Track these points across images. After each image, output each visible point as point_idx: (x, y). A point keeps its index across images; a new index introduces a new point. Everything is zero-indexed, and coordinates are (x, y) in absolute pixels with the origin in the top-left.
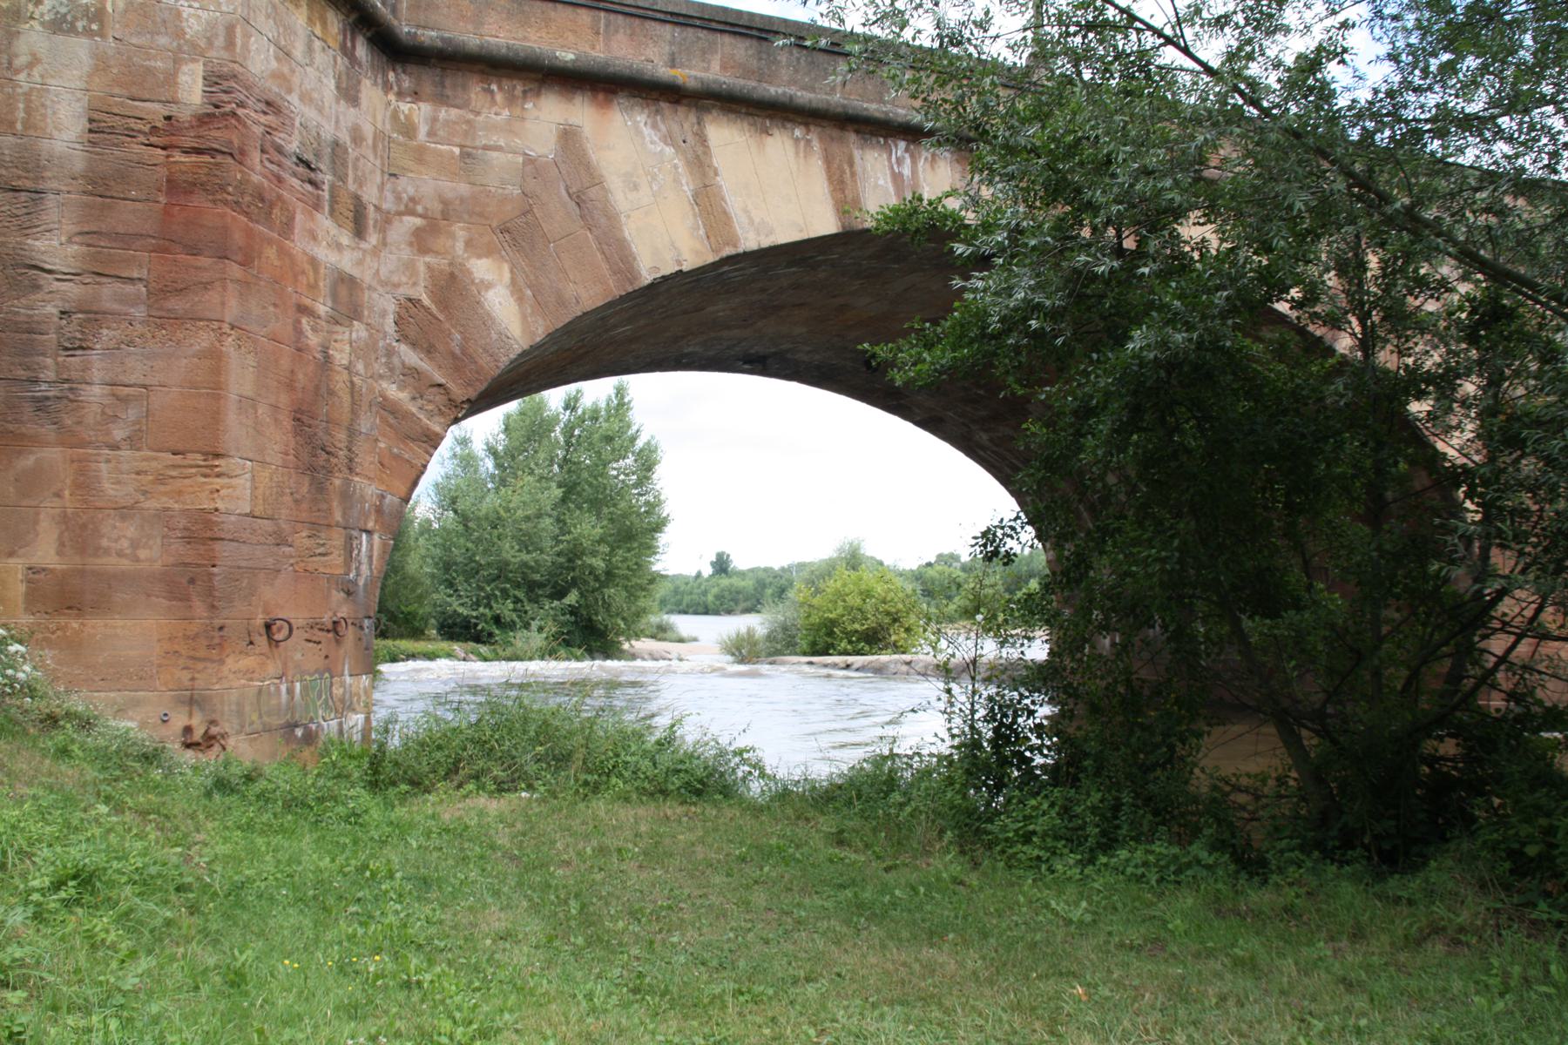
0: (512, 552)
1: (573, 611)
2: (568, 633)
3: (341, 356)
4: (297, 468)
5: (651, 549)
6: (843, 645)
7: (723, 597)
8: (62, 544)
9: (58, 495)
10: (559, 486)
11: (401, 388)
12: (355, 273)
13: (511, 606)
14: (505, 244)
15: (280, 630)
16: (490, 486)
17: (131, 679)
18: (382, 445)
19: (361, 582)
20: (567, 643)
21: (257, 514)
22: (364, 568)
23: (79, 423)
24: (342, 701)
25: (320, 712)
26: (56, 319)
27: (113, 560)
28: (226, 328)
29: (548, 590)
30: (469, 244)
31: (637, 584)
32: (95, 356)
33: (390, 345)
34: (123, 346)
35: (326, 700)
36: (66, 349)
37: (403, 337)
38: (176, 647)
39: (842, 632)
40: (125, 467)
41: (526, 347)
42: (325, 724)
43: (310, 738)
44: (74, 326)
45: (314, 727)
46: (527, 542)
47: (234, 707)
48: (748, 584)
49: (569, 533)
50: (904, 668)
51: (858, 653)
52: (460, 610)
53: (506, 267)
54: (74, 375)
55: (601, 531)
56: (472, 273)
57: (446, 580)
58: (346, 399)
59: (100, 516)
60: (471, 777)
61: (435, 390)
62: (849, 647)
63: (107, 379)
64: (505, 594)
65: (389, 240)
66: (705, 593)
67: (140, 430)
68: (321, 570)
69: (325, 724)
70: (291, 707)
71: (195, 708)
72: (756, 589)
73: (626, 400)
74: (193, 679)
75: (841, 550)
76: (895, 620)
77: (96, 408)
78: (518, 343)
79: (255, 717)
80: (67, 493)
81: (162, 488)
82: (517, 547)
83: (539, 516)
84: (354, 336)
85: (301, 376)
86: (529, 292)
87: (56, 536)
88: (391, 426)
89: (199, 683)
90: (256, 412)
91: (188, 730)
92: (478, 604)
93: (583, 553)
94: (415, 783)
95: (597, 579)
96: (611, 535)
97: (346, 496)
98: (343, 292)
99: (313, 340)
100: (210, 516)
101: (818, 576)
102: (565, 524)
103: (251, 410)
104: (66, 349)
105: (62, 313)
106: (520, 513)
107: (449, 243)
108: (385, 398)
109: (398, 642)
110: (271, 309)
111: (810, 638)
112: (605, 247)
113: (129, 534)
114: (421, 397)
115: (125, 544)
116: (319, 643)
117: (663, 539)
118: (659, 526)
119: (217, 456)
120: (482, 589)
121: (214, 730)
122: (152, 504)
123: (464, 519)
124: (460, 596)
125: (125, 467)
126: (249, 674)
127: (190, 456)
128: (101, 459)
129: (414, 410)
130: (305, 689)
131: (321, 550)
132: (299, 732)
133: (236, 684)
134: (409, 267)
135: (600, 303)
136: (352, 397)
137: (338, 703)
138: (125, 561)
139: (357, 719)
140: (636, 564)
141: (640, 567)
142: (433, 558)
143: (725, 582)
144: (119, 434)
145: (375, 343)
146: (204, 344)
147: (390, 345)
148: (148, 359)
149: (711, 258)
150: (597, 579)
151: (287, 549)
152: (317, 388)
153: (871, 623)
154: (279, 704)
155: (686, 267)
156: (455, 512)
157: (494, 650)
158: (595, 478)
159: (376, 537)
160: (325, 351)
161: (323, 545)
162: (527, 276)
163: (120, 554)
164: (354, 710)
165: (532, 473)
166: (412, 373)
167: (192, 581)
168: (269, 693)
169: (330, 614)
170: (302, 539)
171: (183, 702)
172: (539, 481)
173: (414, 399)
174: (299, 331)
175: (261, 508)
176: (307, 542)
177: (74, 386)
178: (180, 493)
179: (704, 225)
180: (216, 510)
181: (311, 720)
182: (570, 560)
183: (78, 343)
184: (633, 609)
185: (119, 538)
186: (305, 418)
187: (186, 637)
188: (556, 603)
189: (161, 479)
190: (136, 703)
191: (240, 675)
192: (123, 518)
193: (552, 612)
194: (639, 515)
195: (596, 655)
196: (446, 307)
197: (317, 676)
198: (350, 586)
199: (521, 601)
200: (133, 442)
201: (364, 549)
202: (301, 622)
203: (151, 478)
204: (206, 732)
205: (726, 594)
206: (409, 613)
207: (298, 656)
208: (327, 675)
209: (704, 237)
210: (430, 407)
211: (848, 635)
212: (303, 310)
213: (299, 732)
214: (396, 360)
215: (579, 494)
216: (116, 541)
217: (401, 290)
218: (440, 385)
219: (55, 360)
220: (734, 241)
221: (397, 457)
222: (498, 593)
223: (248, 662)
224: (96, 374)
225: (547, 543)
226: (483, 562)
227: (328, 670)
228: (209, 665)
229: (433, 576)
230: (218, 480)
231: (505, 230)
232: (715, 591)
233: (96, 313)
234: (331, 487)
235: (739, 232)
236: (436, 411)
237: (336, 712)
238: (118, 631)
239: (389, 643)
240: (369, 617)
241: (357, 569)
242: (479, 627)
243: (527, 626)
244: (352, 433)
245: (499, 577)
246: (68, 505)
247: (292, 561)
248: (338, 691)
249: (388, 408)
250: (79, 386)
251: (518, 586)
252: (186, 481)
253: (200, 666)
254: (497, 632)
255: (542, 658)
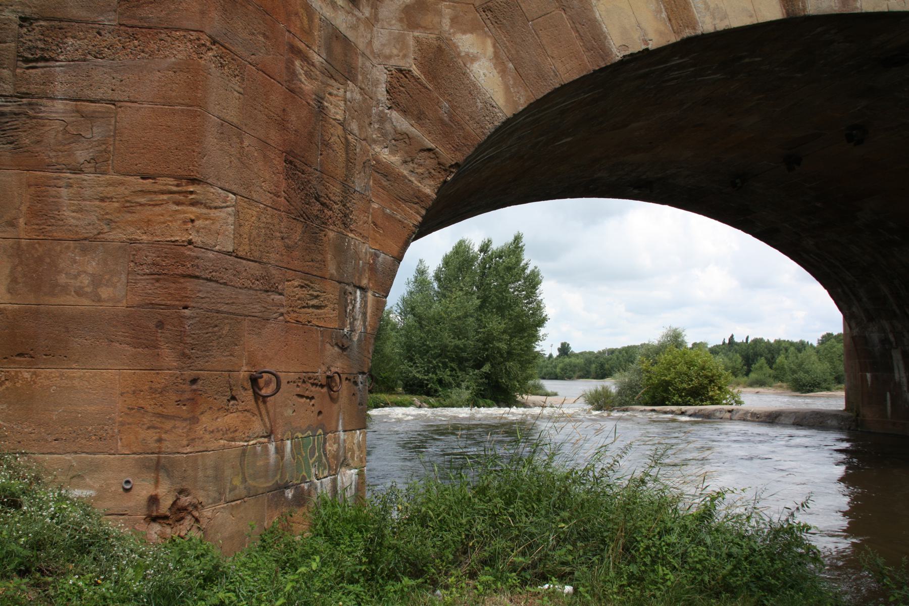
0: (449, 339)
1: (487, 376)
2: (483, 391)
3: (336, 110)
4: (288, 212)
5: (534, 337)
6: (675, 398)
7: (566, 369)
8: (14, 280)
9: (12, 224)
10: (478, 298)
11: (393, 153)
12: (349, 34)
13: (449, 373)
14: (488, 22)
15: (268, 384)
16: (435, 299)
17: (89, 439)
18: (376, 206)
19: (355, 339)
20: (484, 397)
21: (240, 254)
22: (359, 324)
23: (38, 142)
24: (336, 457)
25: (313, 470)
26: (16, 26)
27: (72, 299)
28: (205, 39)
29: (471, 363)
30: (454, 20)
31: (526, 359)
32: (58, 70)
33: (382, 111)
34: (89, 57)
35: (320, 457)
36: (27, 60)
37: (395, 105)
38: (141, 402)
39: (674, 389)
40: (88, 193)
41: (509, 115)
42: (318, 482)
43: (301, 499)
44: (35, 34)
45: (306, 486)
46: (459, 333)
47: (210, 472)
48: (581, 361)
49: (485, 327)
50: (728, 415)
51: (686, 404)
52: (417, 375)
53: (489, 42)
54: (34, 89)
55: (504, 326)
56: (457, 47)
57: (409, 357)
58: (341, 156)
59: (58, 248)
60: (484, 563)
61: (425, 154)
62: (680, 400)
63: (72, 94)
64: (445, 366)
65: (381, 16)
66: (555, 367)
67: (105, 151)
68: (315, 322)
69: (318, 482)
70: (280, 467)
71: (162, 474)
72: (585, 364)
73: (520, 245)
74: (160, 440)
75: (667, 336)
76: (711, 381)
77: (58, 126)
78: (502, 111)
79: (237, 482)
80: (22, 221)
81: (129, 217)
82: (452, 336)
83: (466, 316)
84: (348, 95)
85: (293, 118)
86: (511, 65)
87: (7, 271)
88: (384, 188)
89: (167, 446)
90: (242, 142)
91: (154, 500)
92: (428, 372)
93: (493, 339)
94: (417, 571)
95: (502, 356)
96: (510, 329)
97: (341, 250)
98: (338, 49)
99: (308, 86)
100: (183, 249)
101: (652, 352)
102: (482, 322)
103: (234, 139)
104: (27, 60)
105: (23, 19)
106: (454, 315)
107: (436, 19)
108: (378, 162)
109: (379, 395)
110: (261, 38)
111: (651, 394)
112: (578, 26)
113: (90, 270)
114: (412, 161)
115: (86, 280)
116: (313, 398)
117: (542, 331)
118: (541, 322)
119: (194, 181)
120: (430, 362)
121: (185, 500)
122: (117, 235)
123: (419, 319)
124: (417, 366)
125: (88, 193)
126: (230, 434)
127: (161, 180)
128: (61, 183)
129: (405, 173)
130: (296, 447)
131: (314, 302)
132: (289, 494)
133: (213, 445)
134: (400, 40)
135: (576, 77)
136: (347, 154)
137: (331, 460)
138: (86, 302)
139: (349, 476)
140: (526, 346)
141: (529, 348)
142: (400, 343)
143: (567, 360)
144: (81, 155)
145: (369, 108)
146: (180, 56)
147: (382, 111)
148: (116, 72)
149: (673, 39)
150: (502, 356)
151: (277, 297)
152: (311, 135)
153: (695, 382)
154: (267, 465)
155: (652, 46)
156: (414, 315)
157: (438, 400)
158: (501, 293)
159: (370, 294)
160: (320, 100)
161: (317, 297)
162: (509, 51)
163: (79, 293)
164: (348, 466)
165: (461, 290)
166: (402, 138)
167: (160, 325)
168: (255, 454)
169: (324, 368)
170: (292, 287)
171: (148, 468)
172: (466, 294)
173: (405, 162)
174: (293, 74)
175: (247, 248)
176: (301, 293)
177: (34, 101)
178: (149, 222)
179: (666, 9)
180: (190, 242)
181: (304, 480)
182: (485, 344)
183: (39, 54)
184: (524, 375)
185: (79, 274)
186: (297, 162)
187: (153, 391)
188: (476, 371)
189: (128, 207)
190: (95, 468)
191: (219, 435)
192: (84, 251)
193: (474, 377)
194: (528, 316)
195: (501, 404)
196: (434, 78)
197: (310, 432)
198: (344, 341)
199: (455, 370)
200: (98, 164)
201: (358, 305)
202: (293, 376)
203: (116, 205)
204: (175, 503)
205: (568, 367)
206: (385, 378)
207: (289, 412)
208: (320, 431)
209: (667, 20)
210: (421, 171)
211: (679, 391)
212: (295, 51)
213: (289, 494)
214: (388, 126)
215: (490, 304)
216: (76, 277)
217: (393, 62)
218: (430, 150)
219: (14, 71)
220: (693, 24)
221: (390, 218)
222: (441, 365)
223: (230, 419)
224: (59, 89)
225: (471, 333)
226: (431, 345)
227: (322, 426)
228: (178, 423)
229: (400, 354)
230: (194, 209)
231: (487, 9)
232: (561, 365)
233: (61, 20)
234: (325, 239)
235: (697, 16)
236: (426, 175)
237: (330, 468)
238: (76, 382)
239: (374, 395)
240: (363, 373)
241: (352, 324)
242: (429, 386)
243: (459, 386)
244: (347, 190)
245: (440, 355)
246: (23, 235)
247: (282, 310)
248: (331, 448)
249: (384, 171)
250: (39, 101)
251: (452, 360)
252: (157, 209)
253: (168, 425)
254: (440, 389)
255: (467, 406)
